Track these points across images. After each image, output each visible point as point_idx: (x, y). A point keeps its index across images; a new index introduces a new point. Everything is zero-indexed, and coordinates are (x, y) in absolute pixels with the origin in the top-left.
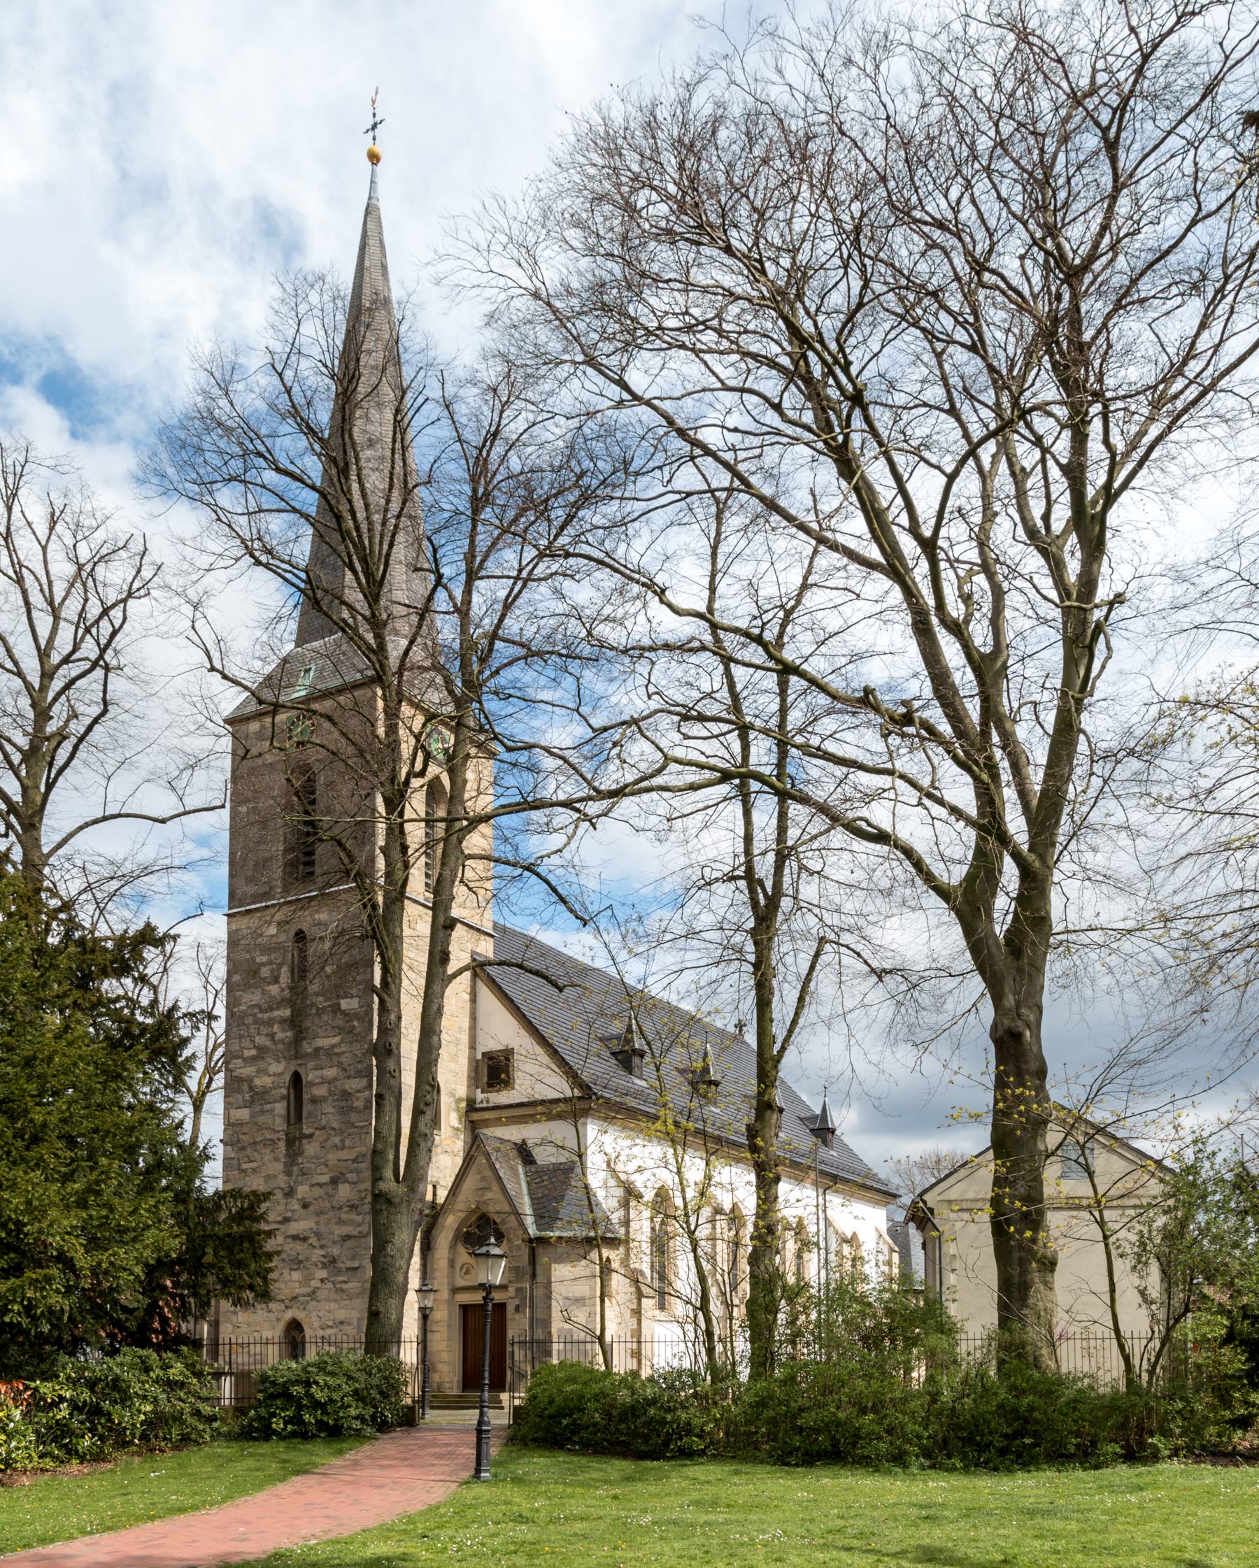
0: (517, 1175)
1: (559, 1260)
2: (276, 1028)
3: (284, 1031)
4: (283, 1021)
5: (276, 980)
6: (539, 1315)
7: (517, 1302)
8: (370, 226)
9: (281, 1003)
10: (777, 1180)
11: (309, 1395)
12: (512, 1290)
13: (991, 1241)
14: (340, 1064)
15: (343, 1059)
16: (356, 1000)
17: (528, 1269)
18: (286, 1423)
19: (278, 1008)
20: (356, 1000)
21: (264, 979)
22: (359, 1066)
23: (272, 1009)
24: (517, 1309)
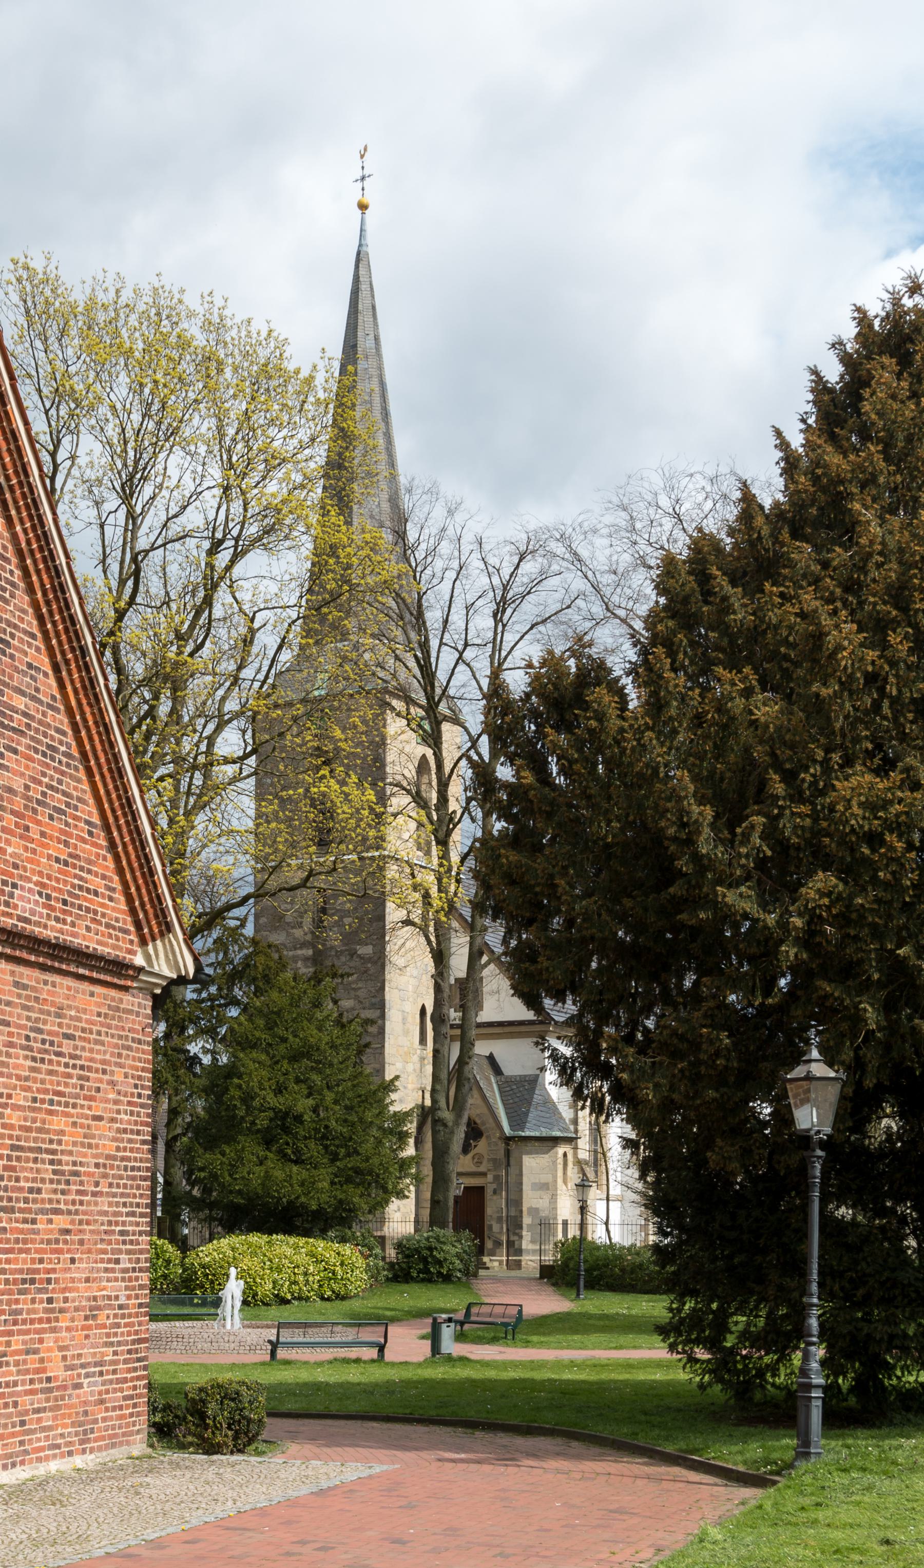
0: (490, 1084)
1: (528, 1153)
2: (300, 964)
3: (307, 967)
4: (306, 959)
5: (300, 925)
6: (512, 1197)
7: (494, 1186)
8: (362, 272)
9: (303, 945)
10: (690, 561)
11: (432, 1256)
12: (490, 1177)
13: (360, 1450)
14: (356, 998)
15: (359, 993)
16: (371, 947)
17: (504, 1161)
18: (418, 1273)
19: (301, 948)
20: (371, 947)
21: (288, 924)
22: (373, 1000)
23: (295, 949)
24: (495, 1192)
